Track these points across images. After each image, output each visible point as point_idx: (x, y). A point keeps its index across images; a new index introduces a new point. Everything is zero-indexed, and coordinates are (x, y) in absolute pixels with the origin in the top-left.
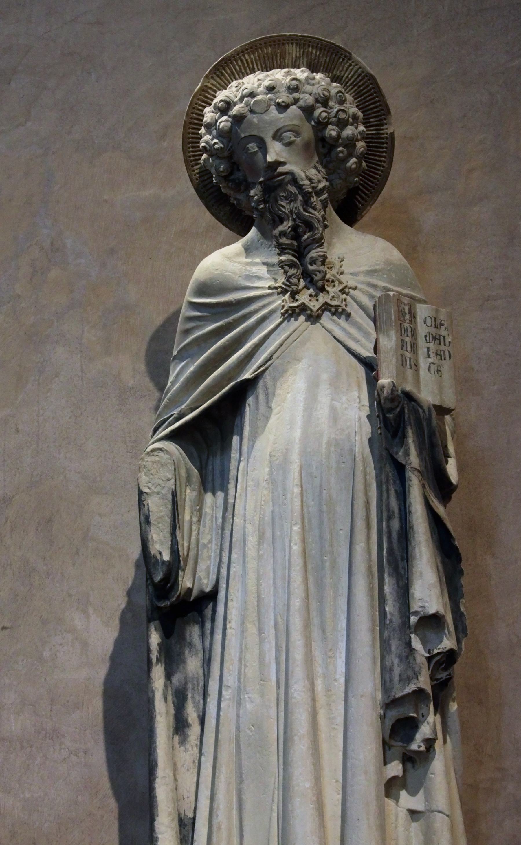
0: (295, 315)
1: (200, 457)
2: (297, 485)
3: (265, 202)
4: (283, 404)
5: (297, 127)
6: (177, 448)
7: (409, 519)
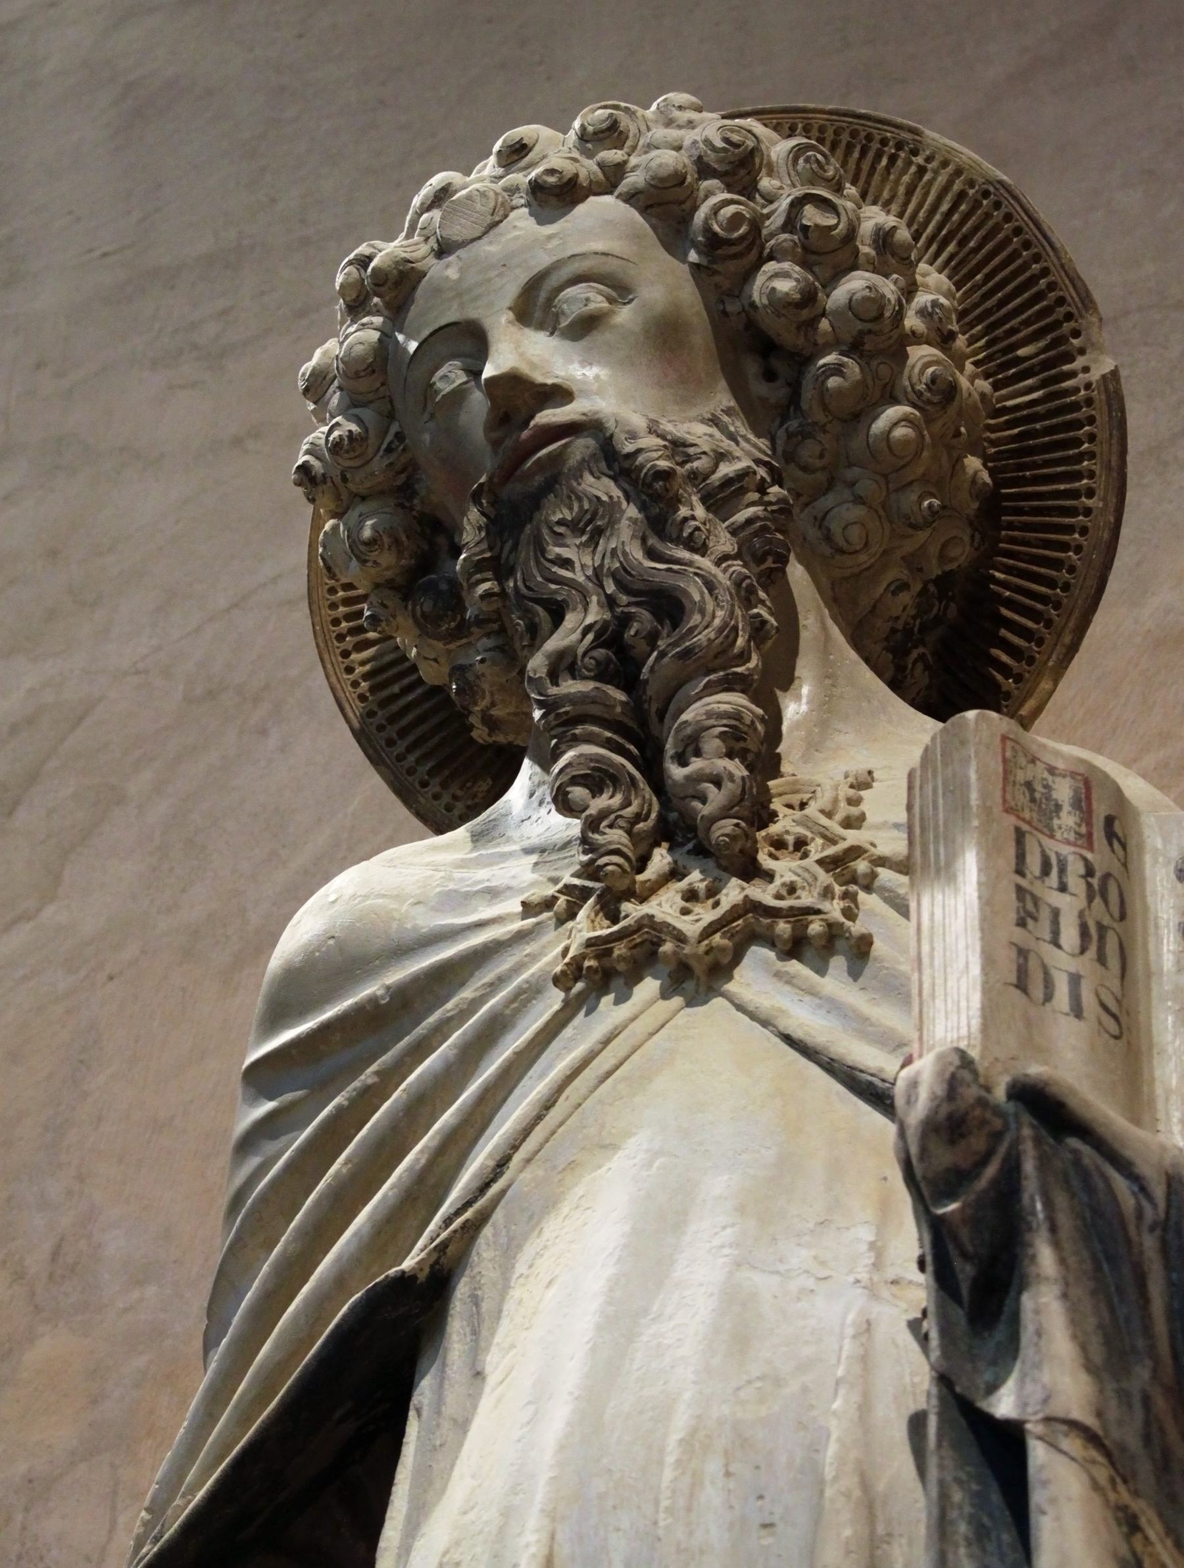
0: (618, 982)
3: (499, 568)
5: (620, 262)
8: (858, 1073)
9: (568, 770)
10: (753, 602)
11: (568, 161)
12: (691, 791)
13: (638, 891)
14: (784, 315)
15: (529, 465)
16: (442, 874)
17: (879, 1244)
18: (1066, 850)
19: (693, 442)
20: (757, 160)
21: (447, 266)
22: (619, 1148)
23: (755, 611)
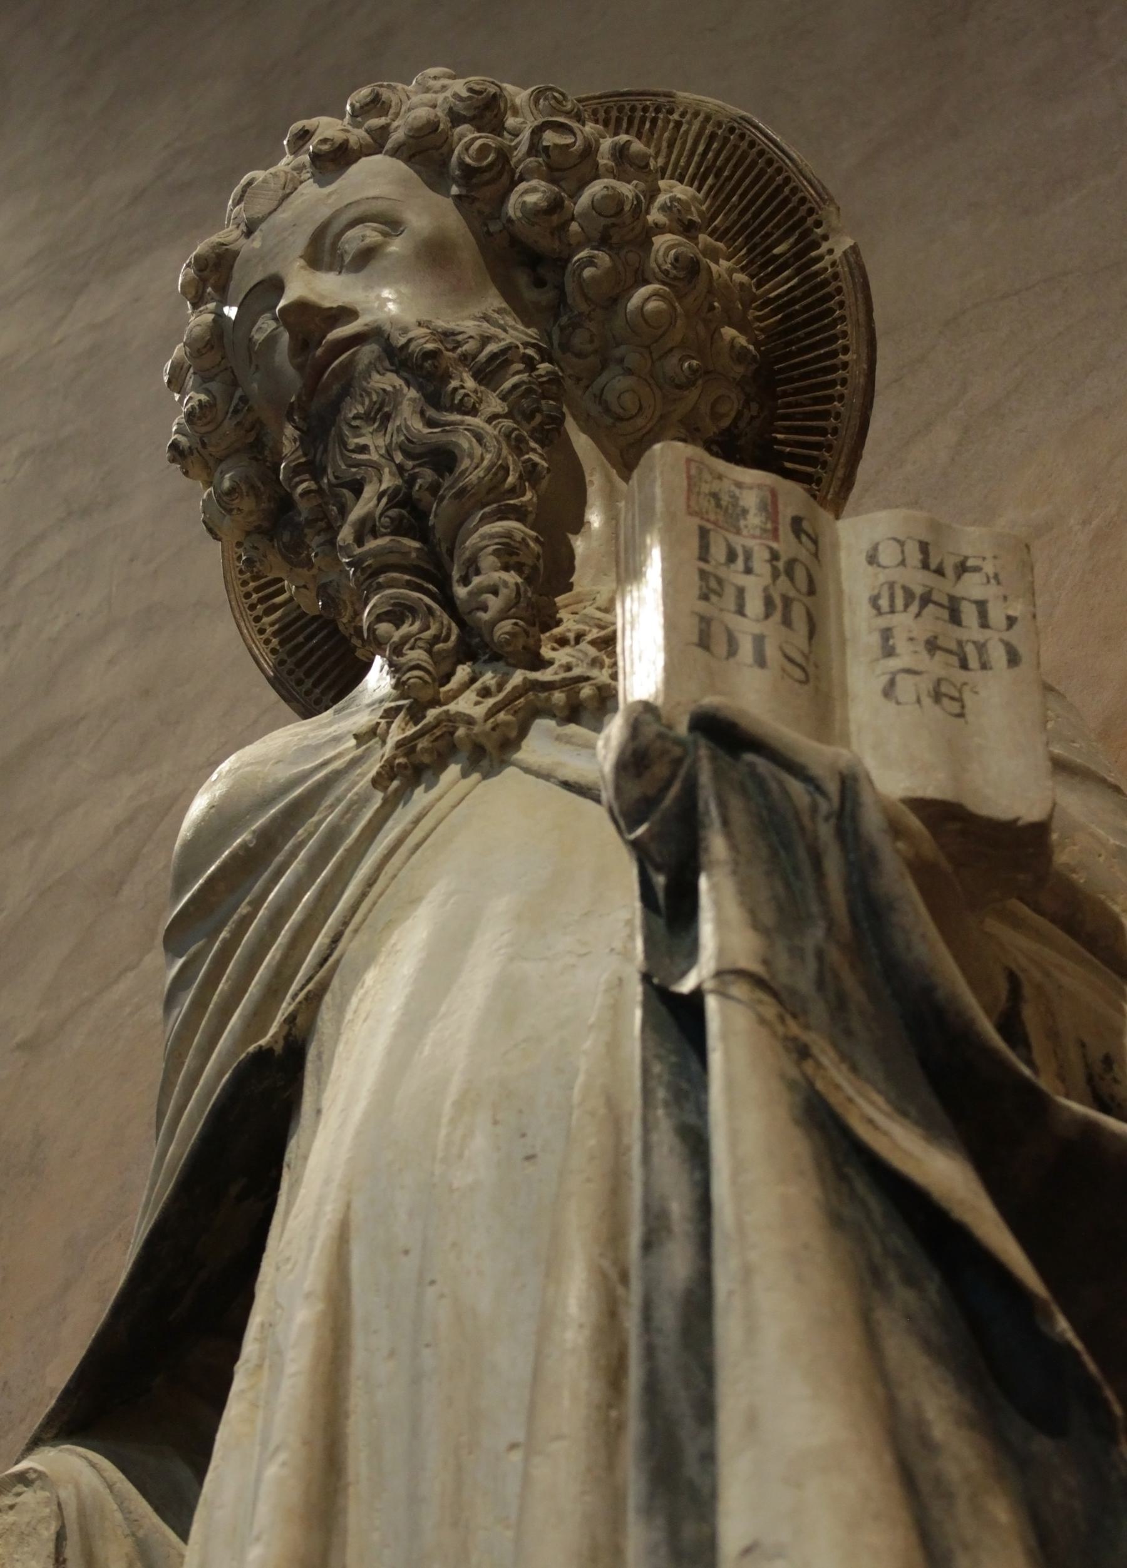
0: (427, 775)
6: (93, 1465)
9: (373, 611)
10: (524, 450)
11: (340, 132)
12: (474, 605)
13: (442, 699)
18: (751, 543)
19: (461, 330)
20: (502, 105)
21: (253, 240)
23: (526, 457)
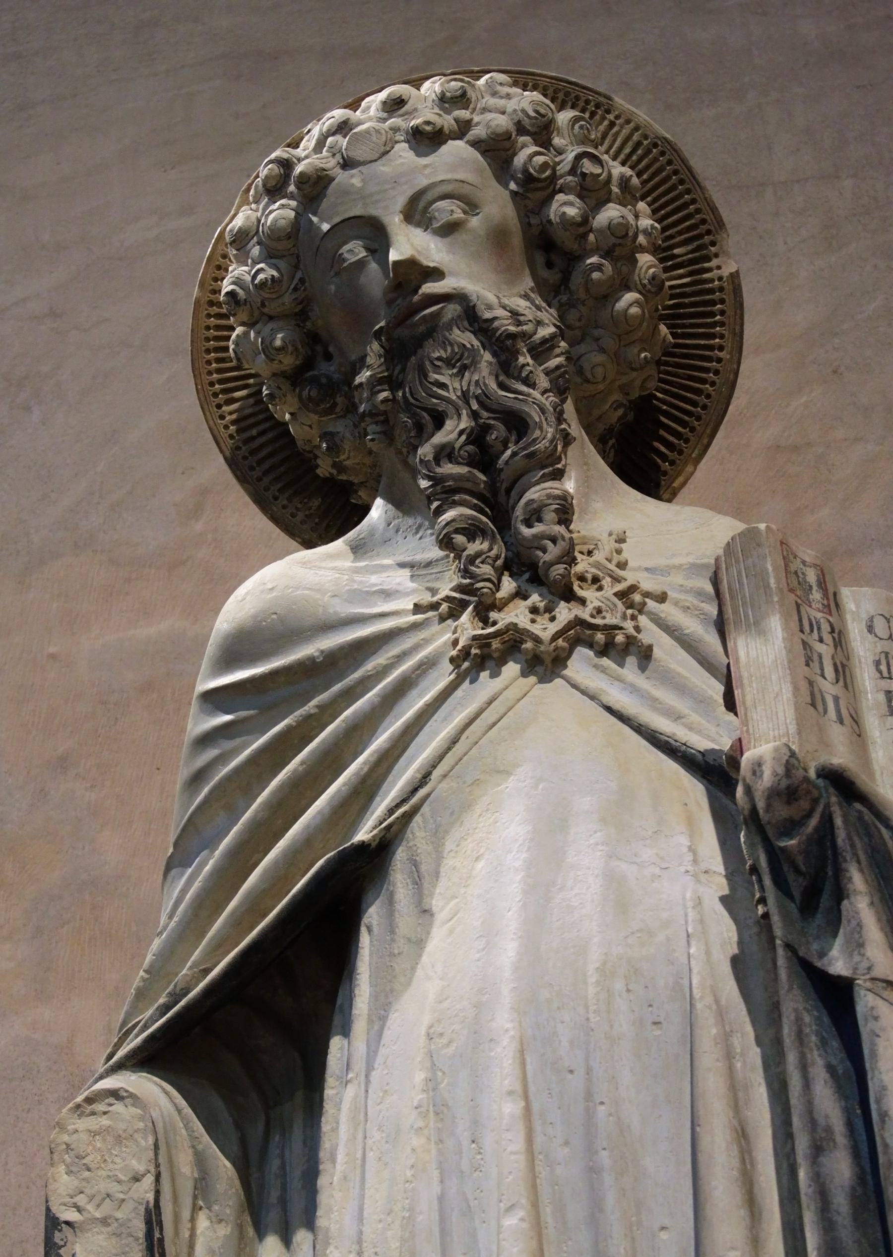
0: (490, 663)
1: (238, 1126)
2: (510, 1093)
3: (393, 384)
4: (463, 890)
6: (166, 1093)
7: (883, 1138)
8: (658, 735)
9: (453, 524)
12: (536, 545)
14: (568, 230)
15: (417, 318)
16: (346, 577)
17: (693, 847)
21: (352, 176)
22: (512, 774)
23: (563, 427)
